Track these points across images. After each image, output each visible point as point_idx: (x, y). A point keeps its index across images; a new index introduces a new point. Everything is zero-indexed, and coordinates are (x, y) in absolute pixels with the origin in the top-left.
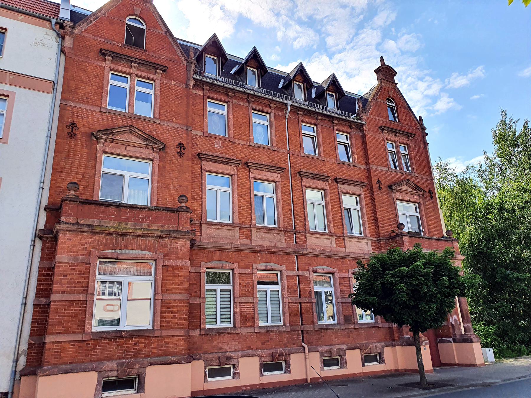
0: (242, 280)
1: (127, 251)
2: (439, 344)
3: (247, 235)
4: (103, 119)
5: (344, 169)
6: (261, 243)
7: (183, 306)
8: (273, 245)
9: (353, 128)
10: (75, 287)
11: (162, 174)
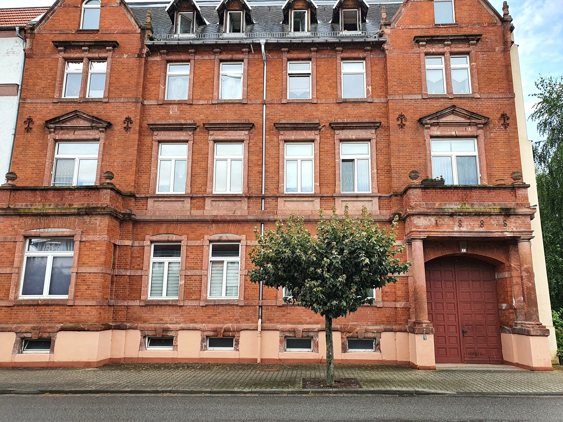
0: (191, 253)
1: (50, 229)
3: (201, 205)
4: (55, 109)
6: (215, 213)
7: (98, 278)
8: (231, 213)
10: (4, 262)
11: (107, 152)
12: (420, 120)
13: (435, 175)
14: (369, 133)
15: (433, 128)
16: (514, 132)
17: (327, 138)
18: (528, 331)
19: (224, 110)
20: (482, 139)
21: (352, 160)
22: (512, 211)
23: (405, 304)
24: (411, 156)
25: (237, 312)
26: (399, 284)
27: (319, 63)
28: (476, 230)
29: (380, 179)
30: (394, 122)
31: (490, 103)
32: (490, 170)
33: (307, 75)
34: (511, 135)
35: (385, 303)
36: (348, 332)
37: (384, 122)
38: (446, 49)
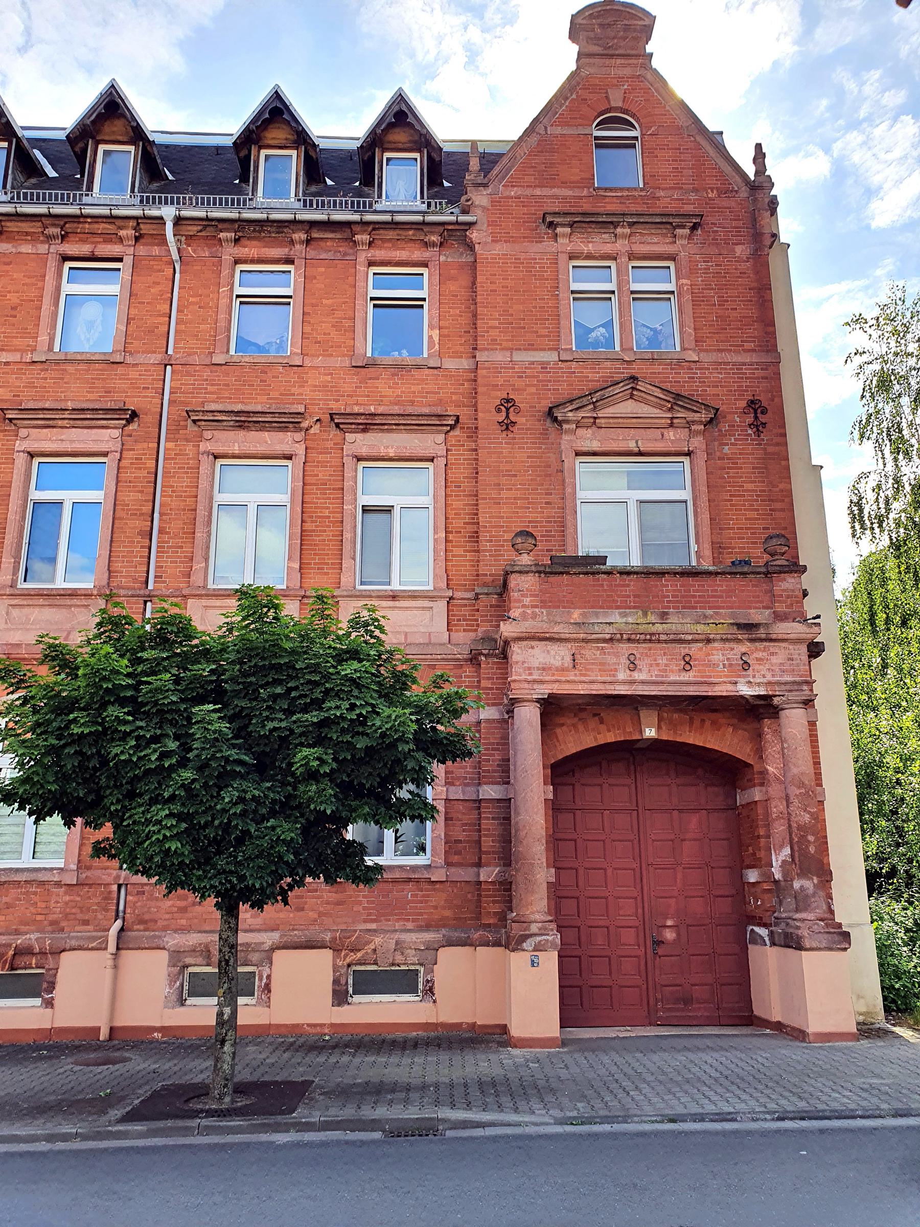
2: (749, 946)
5: (380, 384)
9: (434, 245)
12: (550, 413)
13: (586, 546)
14: (430, 443)
15: (580, 432)
16: (778, 444)
17: (325, 451)
18: (799, 938)
19: (62, 379)
20: (700, 458)
21: (388, 510)
22: (762, 630)
23: (499, 872)
24: (528, 498)
25: (57, 902)
26: (488, 818)
27: (311, 271)
28: (673, 678)
29: (453, 556)
30: (489, 417)
31: (721, 373)
32: (720, 534)
33: (282, 301)
34: (771, 449)
35: (453, 870)
36: (352, 951)
37: (465, 413)
38: (621, 246)
